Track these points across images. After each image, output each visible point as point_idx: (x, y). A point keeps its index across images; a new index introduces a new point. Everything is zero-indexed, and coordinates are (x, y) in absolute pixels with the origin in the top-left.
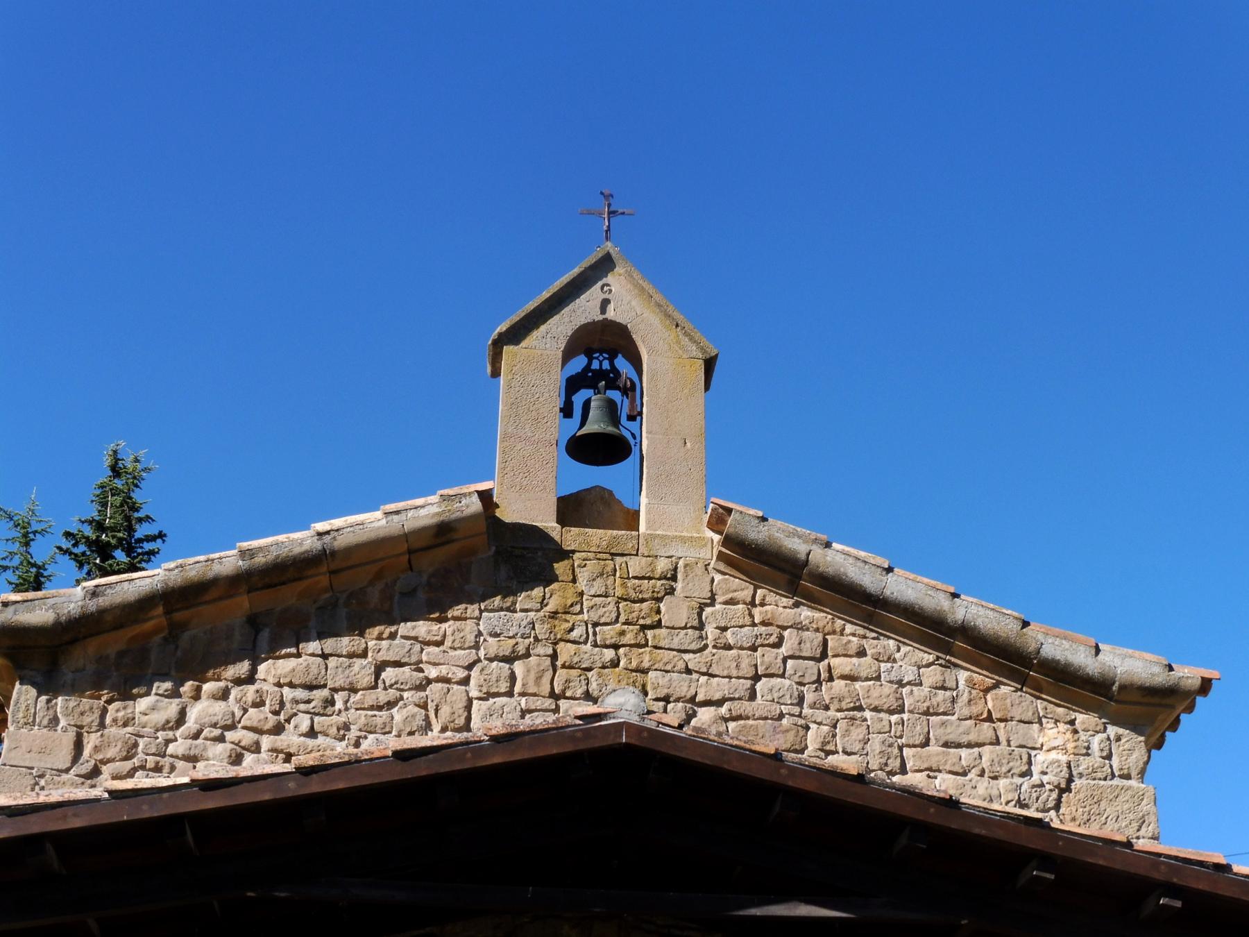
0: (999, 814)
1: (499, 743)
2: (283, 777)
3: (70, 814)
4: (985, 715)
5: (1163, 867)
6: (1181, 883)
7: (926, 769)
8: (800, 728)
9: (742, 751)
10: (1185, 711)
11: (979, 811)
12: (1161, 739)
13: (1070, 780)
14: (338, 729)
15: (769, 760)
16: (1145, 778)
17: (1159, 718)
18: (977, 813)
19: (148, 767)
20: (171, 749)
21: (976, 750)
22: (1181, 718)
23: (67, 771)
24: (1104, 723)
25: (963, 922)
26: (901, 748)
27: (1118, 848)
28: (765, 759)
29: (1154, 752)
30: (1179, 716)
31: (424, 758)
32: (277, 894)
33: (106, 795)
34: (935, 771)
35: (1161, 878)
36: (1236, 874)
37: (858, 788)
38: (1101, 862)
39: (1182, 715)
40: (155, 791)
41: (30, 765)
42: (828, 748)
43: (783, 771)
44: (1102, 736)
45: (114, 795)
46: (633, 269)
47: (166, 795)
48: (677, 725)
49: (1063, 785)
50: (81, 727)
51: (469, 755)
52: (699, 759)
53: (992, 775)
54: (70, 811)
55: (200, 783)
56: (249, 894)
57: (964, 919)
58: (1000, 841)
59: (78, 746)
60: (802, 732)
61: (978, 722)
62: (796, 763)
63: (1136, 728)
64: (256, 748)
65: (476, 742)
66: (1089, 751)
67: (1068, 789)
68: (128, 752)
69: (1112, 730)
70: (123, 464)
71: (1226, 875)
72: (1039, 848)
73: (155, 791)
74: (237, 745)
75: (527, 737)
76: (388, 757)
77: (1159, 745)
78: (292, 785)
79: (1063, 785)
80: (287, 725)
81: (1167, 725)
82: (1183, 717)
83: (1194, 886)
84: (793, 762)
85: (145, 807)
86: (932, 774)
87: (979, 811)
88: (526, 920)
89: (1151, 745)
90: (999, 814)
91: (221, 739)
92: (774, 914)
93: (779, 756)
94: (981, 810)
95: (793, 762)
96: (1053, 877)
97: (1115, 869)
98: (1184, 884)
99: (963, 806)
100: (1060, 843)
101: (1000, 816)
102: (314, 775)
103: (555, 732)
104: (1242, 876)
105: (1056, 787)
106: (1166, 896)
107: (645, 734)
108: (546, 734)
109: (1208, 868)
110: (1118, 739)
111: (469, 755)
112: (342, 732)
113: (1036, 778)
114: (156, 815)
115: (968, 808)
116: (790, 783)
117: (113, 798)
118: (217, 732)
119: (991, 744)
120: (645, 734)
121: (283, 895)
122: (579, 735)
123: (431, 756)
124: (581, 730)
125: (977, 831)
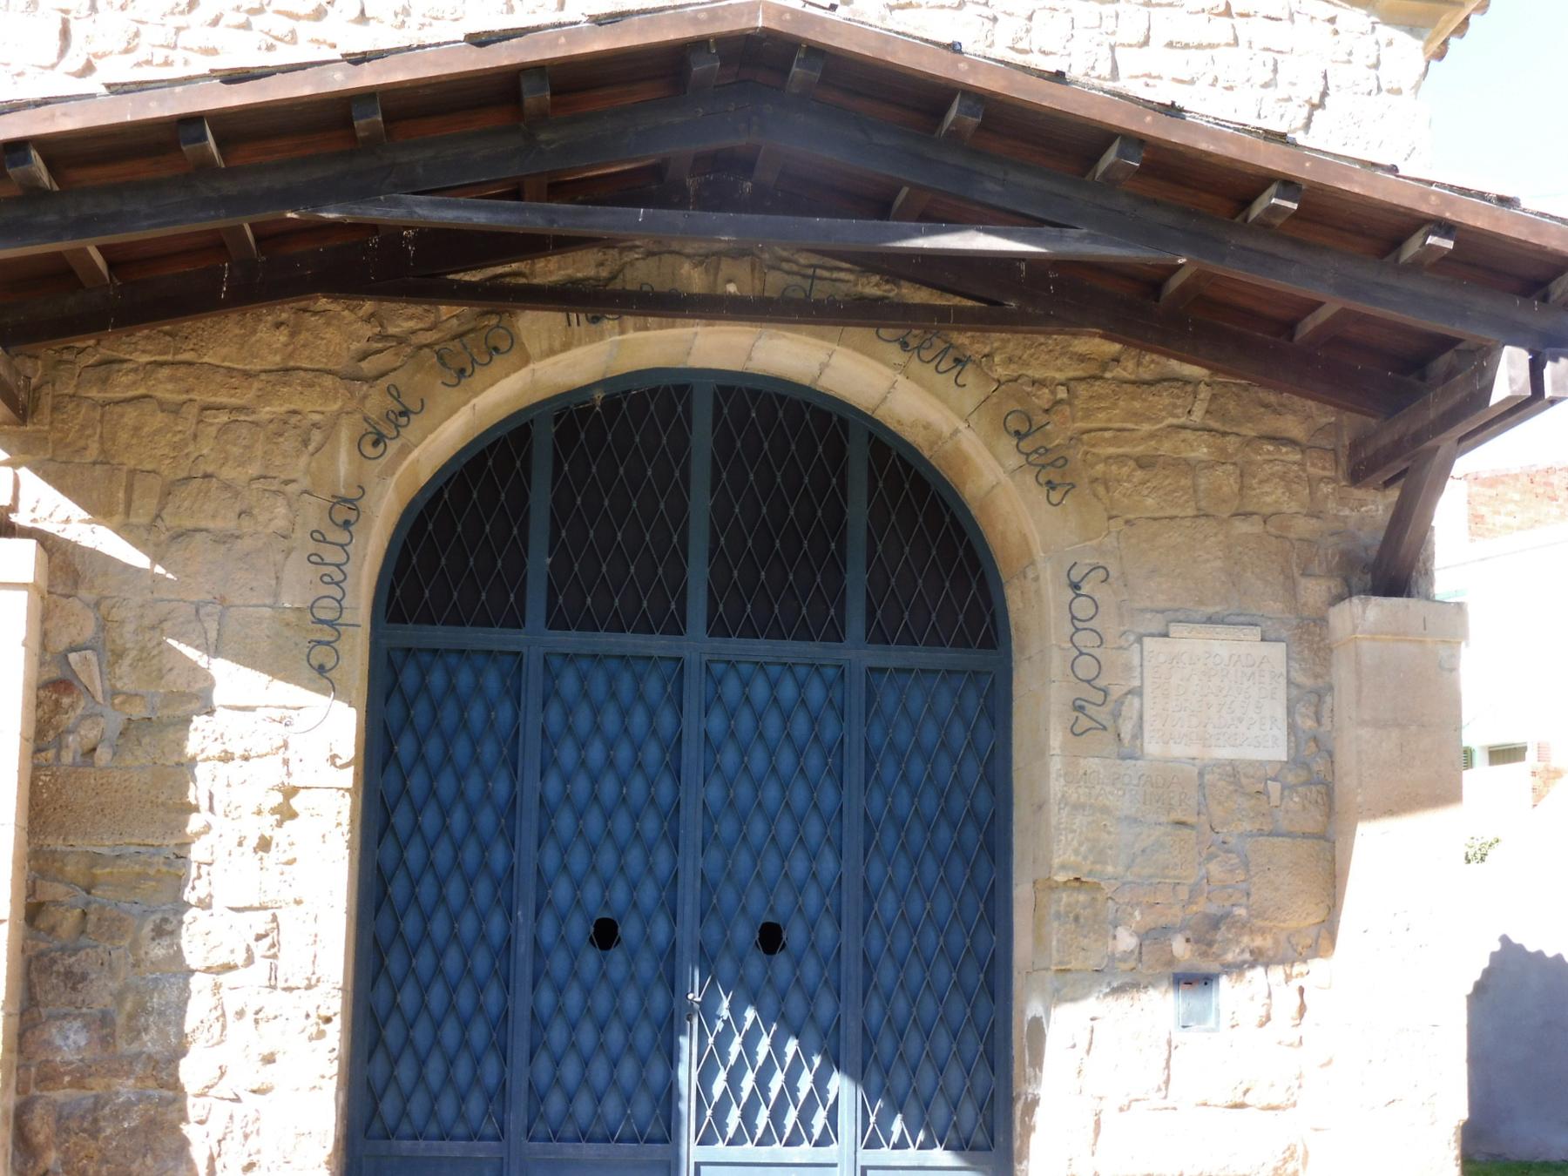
0: (1232, 126)
1: (600, 25)
2: (326, 66)
3: (58, 113)
4: (1222, 8)
5: (1433, 198)
6: (1454, 218)
7: (1145, 75)
8: (985, 20)
9: (910, 40)
10: (1475, 10)
11: (1208, 122)
12: (1443, 47)
13: (1324, 94)
14: (396, 14)
15: (945, 52)
16: (1419, 94)
17: (1442, 18)
18: (1205, 124)
19: (155, 62)
20: (184, 39)
21: (1209, 52)
22: (1471, 20)
23: (53, 67)
24: (1373, 23)
25: (1180, 261)
26: (1112, 48)
27: (1379, 173)
28: (940, 50)
29: (1433, 63)
30: (1467, 18)
31: (505, 43)
32: (325, 215)
33: (104, 91)
34: (1155, 78)
35: (1431, 212)
36: (1524, 210)
37: (1055, 88)
38: (1357, 190)
39: (1472, 16)
40: (164, 84)
41: (6, 62)
42: (1019, 46)
43: (963, 66)
44: (1371, 39)
45: (113, 89)
46: (792, 1046)
47: (178, 89)
48: (828, 6)
49: (1316, 100)
50: (66, 12)
51: (562, 40)
52: (856, 50)
53: (1227, 85)
54: (57, 108)
55: (222, 73)
56: (290, 215)
57: (1181, 256)
58: (1232, 160)
59: (65, 34)
60: (988, 24)
61: (1212, 17)
62: (979, 56)
63: (1413, 29)
64: (293, 39)
65: (572, 24)
66: (1351, 58)
67: (1321, 105)
68: (129, 43)
69: (1385, 32)
70: (164, 986)
71: (1512, 210)
72: (1280, 170)
73: (164, 84)
74: (267, 33)
75: (637, 18)
76: (460, 42)
77: (1440, 55)
78: (338, 76)
79: (1316, 100)
80: (329, 8)
81: (1452, 28)
82: (1475, 20)
83: (1471, 222)
84: (975, 55)
85: (153, 104)
86: (1151, 82)
87: (1208, 122)
88: (636, 256)
89: (1431, 52)
90: (1232, 126)
91: (246, 26)
92: (946, 247)
93: (958, 47)
94: (1211, 120)
95: (975, 55)
96: (1295, 206)
97: (1374, 199)
98: (1459, 220)
99: (1188, 114)
100: (1307, 165)
101: (1235, 129)
102: (366, 63)
103: (672, 11)
104: (1532, 213)
105: (1306, 101)
106: (1435, 234)
107: (788, 17)
108: (660, 14)
109: (1489, 201)
110: (1390, 44)
111: (562, 40)
112: (401, 17)
113: (1282, 91)
114: (167, 114)
115: (1194, 118)
116: (971, 82)
117: (112, 93)
118: (242, 18)
119: (1228, 45)
120: (788, 17)
121: (331, 216)
122: (703, 16)
123: (514, 40)
124: (706, 10)
125: (1203, 146)
